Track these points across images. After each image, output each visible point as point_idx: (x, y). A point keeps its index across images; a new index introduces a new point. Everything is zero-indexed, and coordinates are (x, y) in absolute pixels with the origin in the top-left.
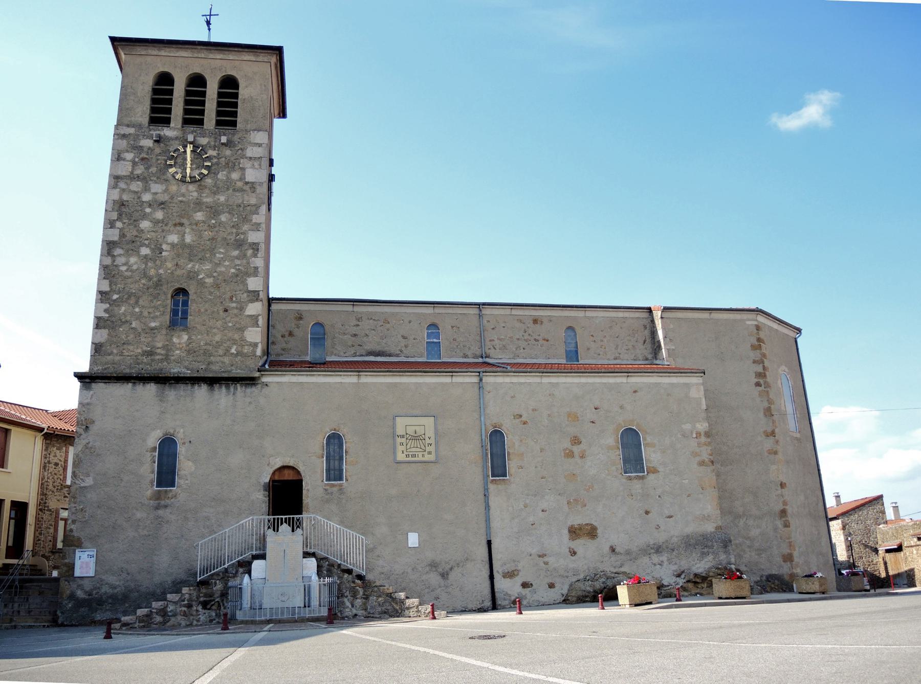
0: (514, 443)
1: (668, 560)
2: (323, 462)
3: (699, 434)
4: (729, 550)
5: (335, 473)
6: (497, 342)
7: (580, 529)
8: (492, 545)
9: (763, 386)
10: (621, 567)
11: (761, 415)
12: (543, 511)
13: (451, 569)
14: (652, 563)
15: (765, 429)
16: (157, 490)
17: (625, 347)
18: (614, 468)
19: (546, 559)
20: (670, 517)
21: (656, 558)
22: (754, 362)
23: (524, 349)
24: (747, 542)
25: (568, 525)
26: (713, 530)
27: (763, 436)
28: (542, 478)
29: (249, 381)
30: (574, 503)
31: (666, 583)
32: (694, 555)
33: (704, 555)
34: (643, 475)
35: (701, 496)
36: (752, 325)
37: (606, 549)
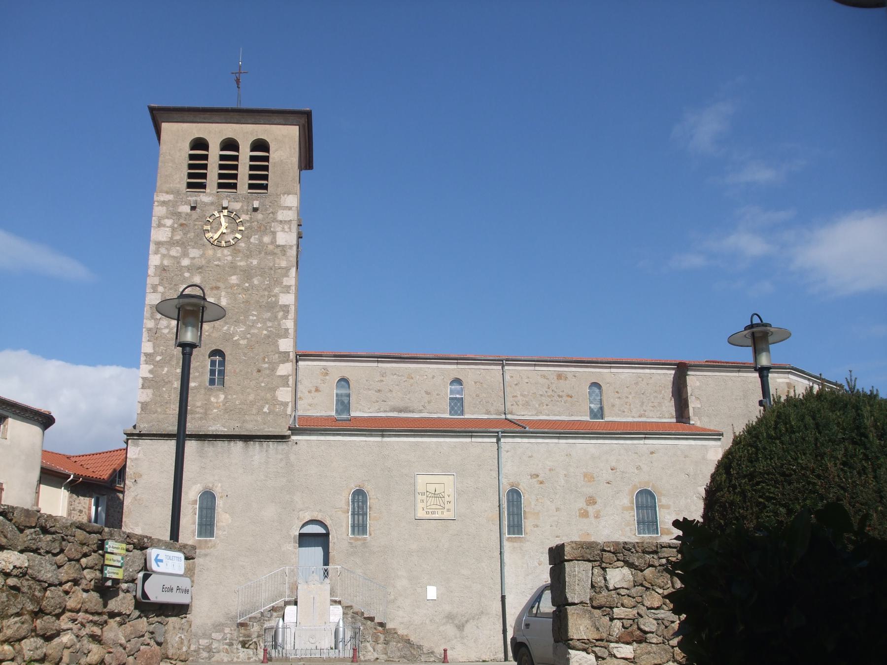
5: (359, 527)
13: (467, 621)
18: (628, 529)
23: (547, 405)
28: (557, 537)
34: (657, 537)
36: (783, 383)
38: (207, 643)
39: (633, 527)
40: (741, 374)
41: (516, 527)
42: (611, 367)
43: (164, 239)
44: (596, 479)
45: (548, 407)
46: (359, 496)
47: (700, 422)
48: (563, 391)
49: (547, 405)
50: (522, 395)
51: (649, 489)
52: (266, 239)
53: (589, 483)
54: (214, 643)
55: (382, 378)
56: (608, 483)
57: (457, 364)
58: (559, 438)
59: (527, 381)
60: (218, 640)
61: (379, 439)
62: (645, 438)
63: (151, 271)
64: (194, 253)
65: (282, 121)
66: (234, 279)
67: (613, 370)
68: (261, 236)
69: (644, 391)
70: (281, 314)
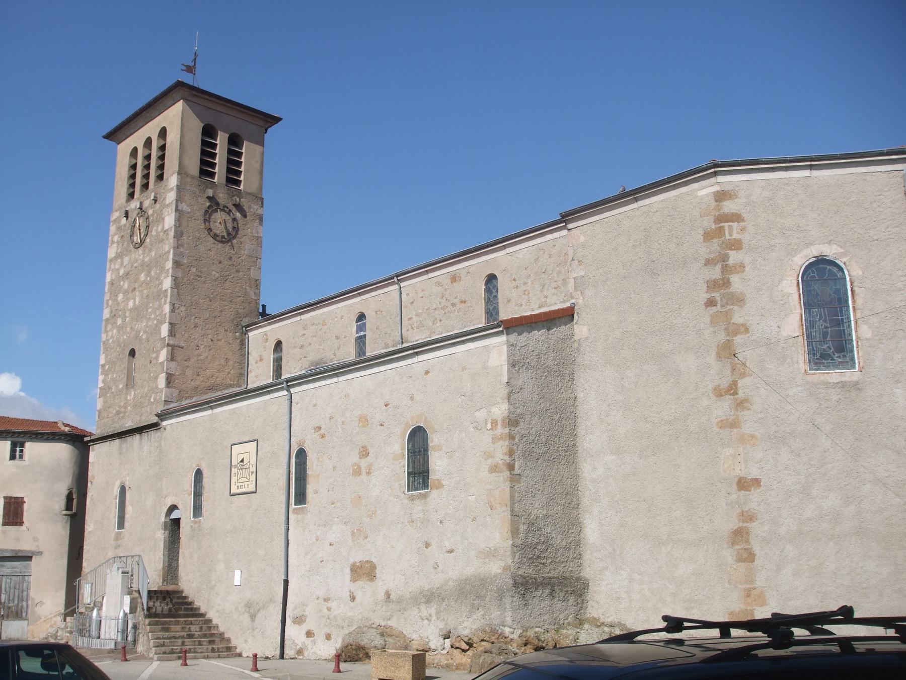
0: (313, 463)
1: (437, 613)
2: (191, 498)
3: (495, 423)
4: (505, 604)
5: (197, 510)
6: (415, 319)
7: (361, 567)
8: (289, 587)
9: (719, 305)
10: (389, 619)
11: (712, 358)
12: (331, 545)
13: (259, 610)
14: (420, 616)
15: (717, 384)
16: (117, 532)
17: (554, 285)
18: (397, 485)
19: (330, 604)
20: (451, 551)
21: (425, 611)
22: (708, 263)
23: (440, 321)
24: (671, 587)
25: (351, 563)
26: (500, 571)
27: (712, 395)
28: (332, 504)
29: (154, 426)
30: (359, 534)
31: (433, 647)
32: (463, 608)
33: (474, 608)
34: (426, 493)
35: (488, 519)
36: (707, 195)
37: (381, 595)
38: (54, 631)
39: (402, 482)
40: (641, 203)
41: (301, 497)
42: (505, 247)
44: (370, 422)
45: (442, 322)
46: (199, 474)
47: (583, 299)
48: (456, 297)
49: (440, 321)
50: (417, 315)
51: (422, 425)
53: (363, 428)
54: (59, 631)
55: (305, 332)
56: (382, 425)
57: (360, 294)
58: (337, 375)
59: (421, 295)
60: (62, 629)
61: (209, 412)
62: (417, 354)
65: (171, 102)
67: (509, 250)
69: (545, 267)
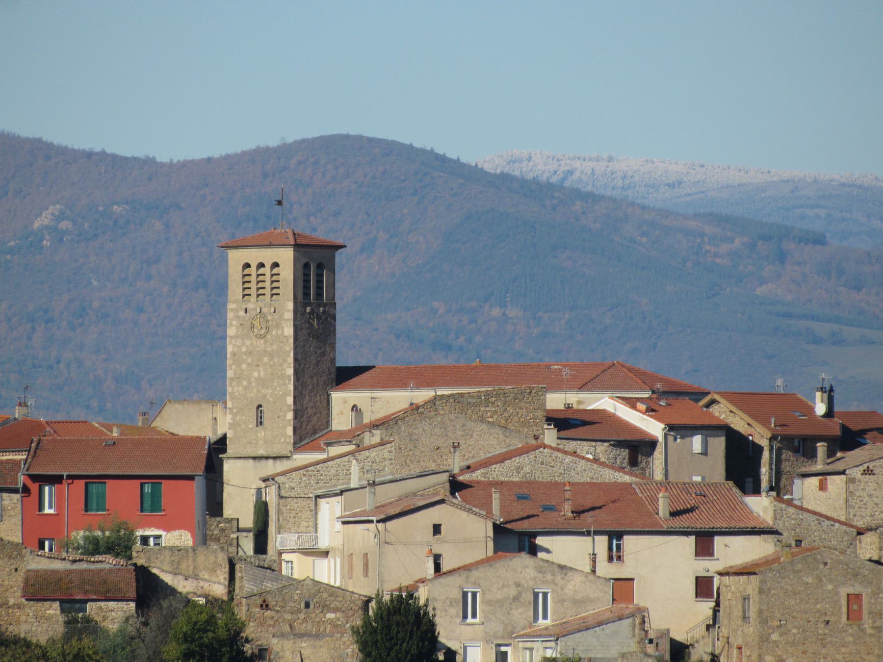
43: (233, 335)
52: (280, 332)
63: (228, 356)
64: (248, 342)
66: (266, 359)
68: (277, 331)
70: (287, 381)
